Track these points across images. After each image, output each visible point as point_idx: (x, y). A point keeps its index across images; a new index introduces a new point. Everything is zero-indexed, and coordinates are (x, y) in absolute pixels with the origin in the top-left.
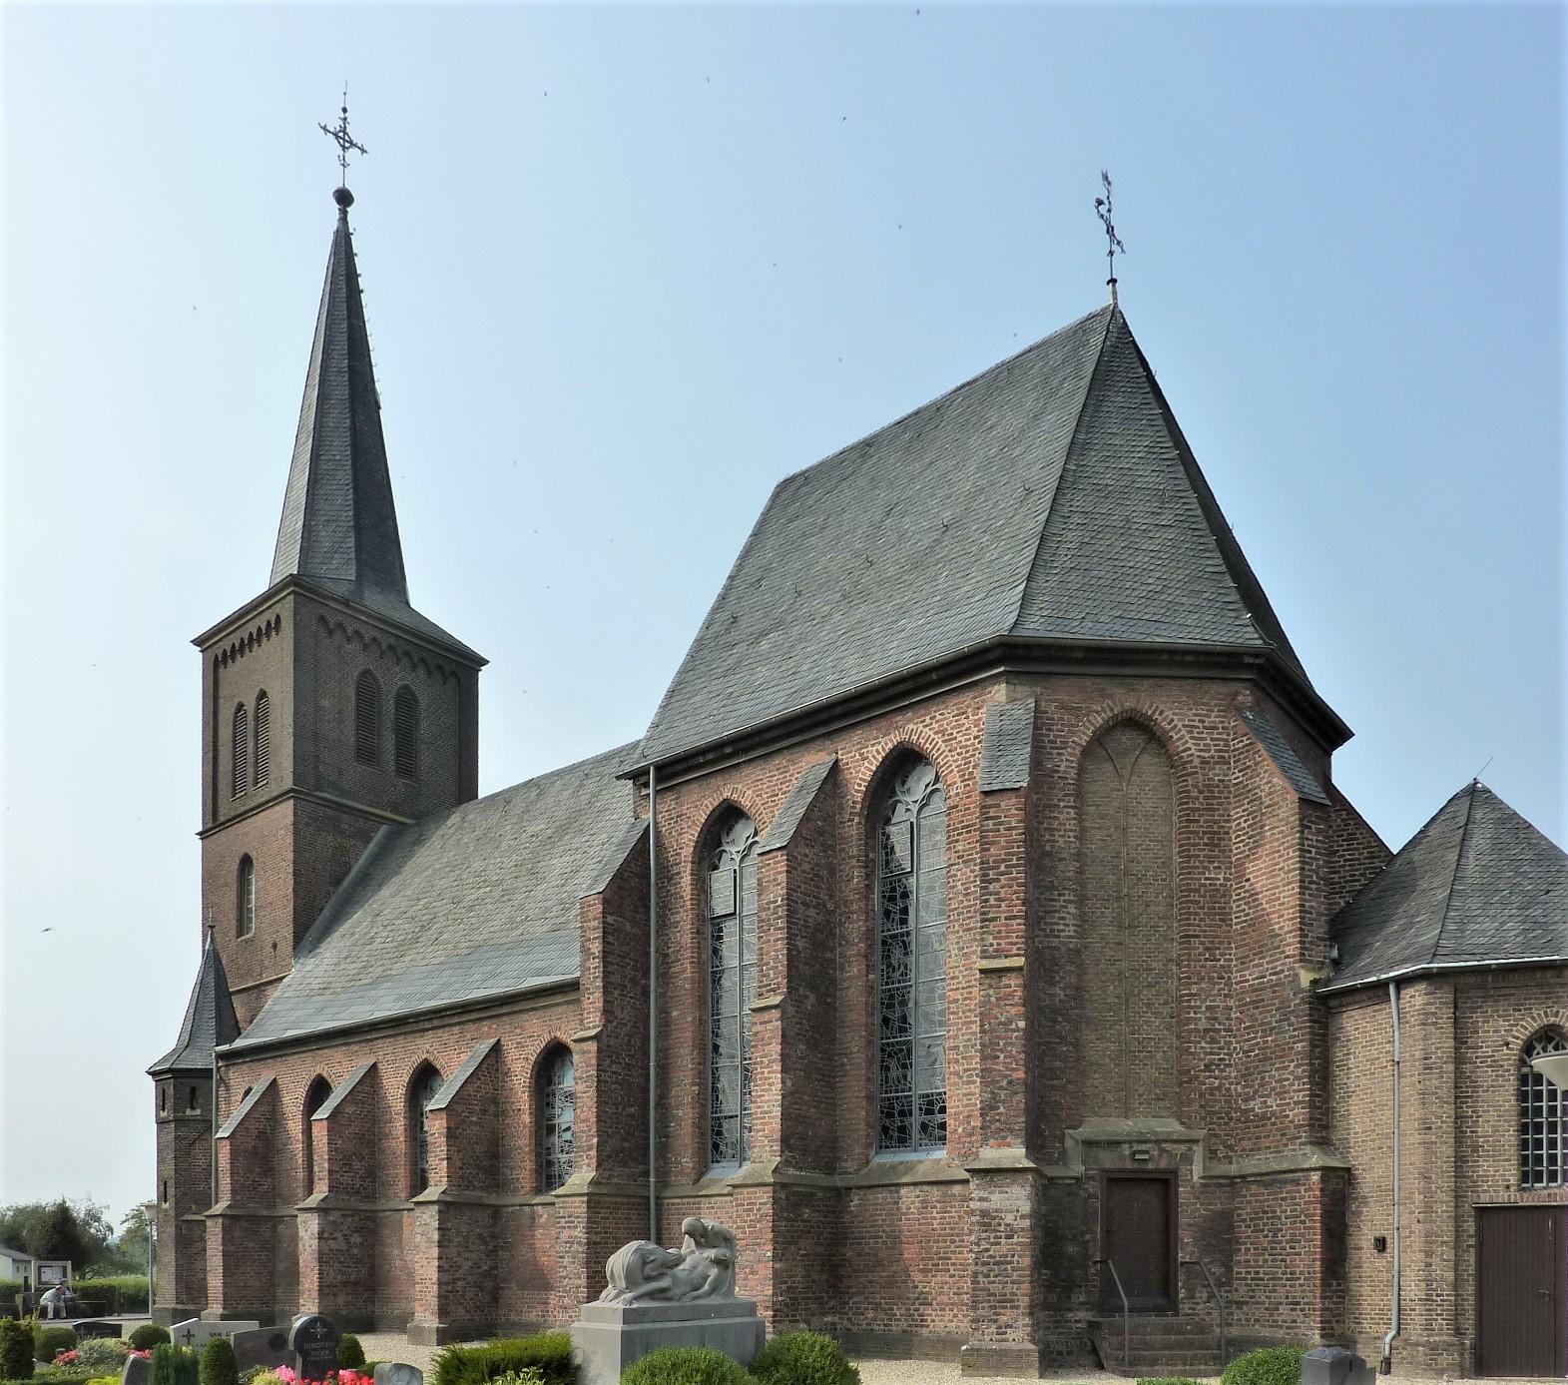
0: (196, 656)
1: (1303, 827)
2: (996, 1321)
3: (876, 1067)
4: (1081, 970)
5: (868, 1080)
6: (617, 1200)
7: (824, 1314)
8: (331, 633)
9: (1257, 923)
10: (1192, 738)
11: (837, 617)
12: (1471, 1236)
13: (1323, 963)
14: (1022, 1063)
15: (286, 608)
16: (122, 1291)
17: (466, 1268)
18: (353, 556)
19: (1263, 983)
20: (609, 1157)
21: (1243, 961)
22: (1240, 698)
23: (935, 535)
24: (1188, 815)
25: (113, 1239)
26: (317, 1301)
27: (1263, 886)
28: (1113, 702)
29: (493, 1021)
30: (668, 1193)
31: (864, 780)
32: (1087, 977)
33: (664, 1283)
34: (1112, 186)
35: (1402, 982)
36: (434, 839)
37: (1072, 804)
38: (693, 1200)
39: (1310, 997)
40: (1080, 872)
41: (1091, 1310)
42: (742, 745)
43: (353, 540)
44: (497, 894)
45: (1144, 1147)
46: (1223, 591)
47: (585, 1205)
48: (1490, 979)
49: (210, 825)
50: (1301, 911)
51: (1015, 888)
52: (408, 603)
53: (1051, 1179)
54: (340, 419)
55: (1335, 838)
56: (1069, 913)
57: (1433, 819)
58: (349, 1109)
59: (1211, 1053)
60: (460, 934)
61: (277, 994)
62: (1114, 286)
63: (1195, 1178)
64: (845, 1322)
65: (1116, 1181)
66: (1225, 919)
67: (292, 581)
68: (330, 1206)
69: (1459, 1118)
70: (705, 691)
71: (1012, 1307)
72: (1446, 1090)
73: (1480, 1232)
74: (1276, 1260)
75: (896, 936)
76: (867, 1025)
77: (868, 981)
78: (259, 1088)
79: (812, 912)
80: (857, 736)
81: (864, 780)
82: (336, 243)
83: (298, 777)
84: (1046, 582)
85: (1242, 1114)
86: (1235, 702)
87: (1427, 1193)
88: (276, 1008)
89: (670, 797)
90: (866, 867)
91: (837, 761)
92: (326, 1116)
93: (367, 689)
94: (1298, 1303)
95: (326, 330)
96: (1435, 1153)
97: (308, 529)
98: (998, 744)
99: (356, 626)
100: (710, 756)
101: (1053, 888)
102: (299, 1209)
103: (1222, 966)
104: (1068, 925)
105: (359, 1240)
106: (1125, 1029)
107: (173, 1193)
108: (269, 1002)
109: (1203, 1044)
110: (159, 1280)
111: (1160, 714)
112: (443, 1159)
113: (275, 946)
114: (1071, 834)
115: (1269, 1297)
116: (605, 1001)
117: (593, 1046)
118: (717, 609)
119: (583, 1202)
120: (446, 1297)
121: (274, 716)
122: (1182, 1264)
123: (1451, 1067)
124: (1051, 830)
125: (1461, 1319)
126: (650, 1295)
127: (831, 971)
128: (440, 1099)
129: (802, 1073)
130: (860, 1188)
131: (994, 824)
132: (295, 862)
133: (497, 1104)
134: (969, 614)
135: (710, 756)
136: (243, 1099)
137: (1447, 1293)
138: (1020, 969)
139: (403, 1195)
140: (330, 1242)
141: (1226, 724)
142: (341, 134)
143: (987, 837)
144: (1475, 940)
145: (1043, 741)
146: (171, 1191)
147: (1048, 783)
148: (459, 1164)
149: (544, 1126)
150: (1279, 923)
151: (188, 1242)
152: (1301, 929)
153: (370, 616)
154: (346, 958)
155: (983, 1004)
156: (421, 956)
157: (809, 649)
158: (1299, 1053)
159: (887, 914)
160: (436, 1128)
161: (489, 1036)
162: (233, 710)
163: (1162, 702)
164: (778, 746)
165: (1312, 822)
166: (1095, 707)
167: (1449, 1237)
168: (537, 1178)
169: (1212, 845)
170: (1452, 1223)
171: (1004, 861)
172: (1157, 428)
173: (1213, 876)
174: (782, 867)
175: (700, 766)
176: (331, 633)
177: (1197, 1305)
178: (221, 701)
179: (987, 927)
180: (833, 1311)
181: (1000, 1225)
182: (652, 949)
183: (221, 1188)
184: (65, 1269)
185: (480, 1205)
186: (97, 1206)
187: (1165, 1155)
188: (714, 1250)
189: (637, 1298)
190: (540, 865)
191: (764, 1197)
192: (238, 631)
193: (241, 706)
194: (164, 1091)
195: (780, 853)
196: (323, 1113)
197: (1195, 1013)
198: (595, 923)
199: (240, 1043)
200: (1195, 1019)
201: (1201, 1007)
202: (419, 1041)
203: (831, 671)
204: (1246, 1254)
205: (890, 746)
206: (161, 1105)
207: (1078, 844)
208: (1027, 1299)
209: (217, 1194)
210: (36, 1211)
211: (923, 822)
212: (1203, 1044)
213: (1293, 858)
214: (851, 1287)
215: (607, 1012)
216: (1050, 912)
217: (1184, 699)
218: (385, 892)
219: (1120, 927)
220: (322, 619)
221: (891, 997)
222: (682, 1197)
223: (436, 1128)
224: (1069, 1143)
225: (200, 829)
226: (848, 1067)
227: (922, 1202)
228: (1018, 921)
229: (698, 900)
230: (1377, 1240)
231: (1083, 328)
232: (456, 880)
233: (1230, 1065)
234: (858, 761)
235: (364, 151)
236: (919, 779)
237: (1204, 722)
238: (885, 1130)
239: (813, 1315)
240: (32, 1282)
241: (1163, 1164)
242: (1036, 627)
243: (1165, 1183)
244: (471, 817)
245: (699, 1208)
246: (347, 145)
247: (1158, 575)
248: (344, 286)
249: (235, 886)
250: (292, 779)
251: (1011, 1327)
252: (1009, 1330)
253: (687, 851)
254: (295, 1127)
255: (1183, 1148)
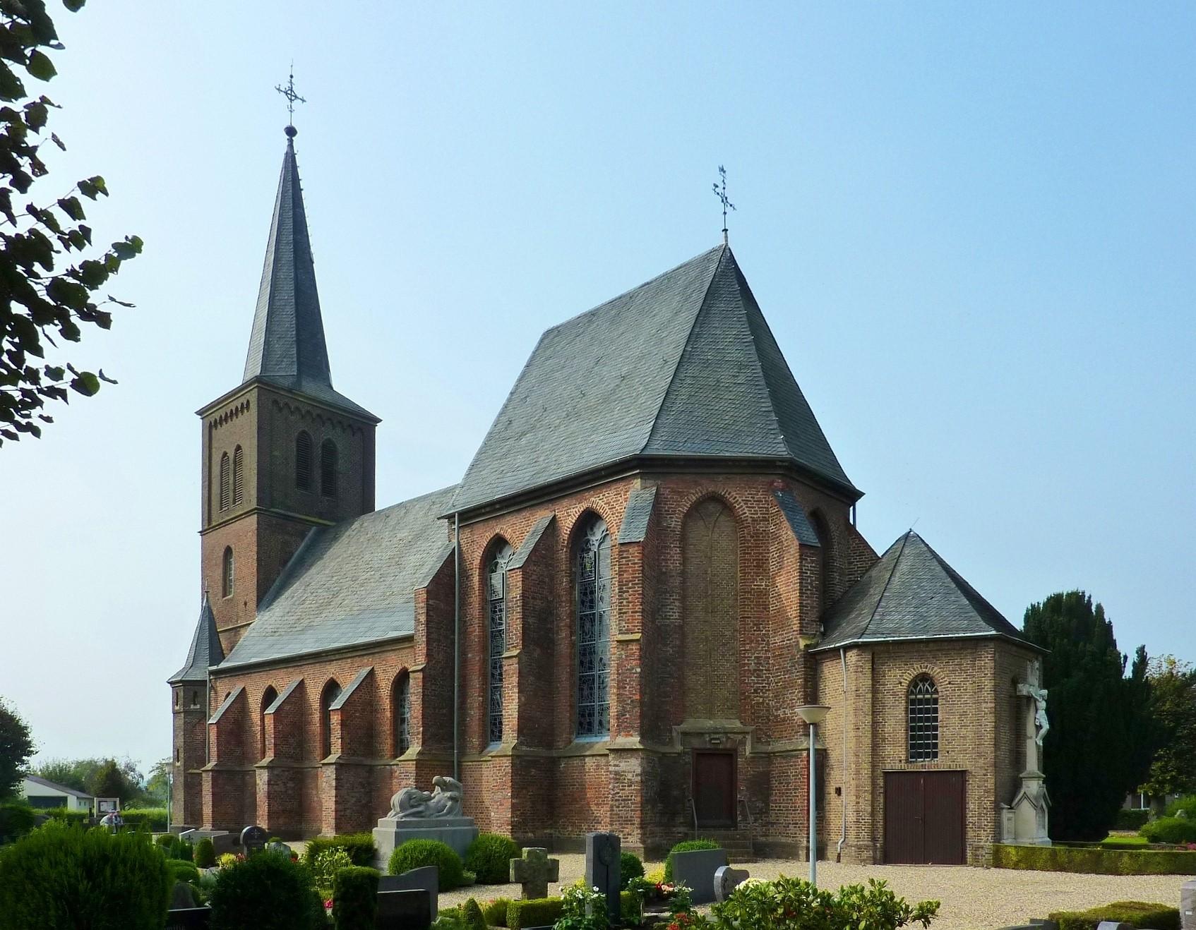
0: (198, 421)
1: (801, 559)
2: (622, 831)
3: (576, 689)
4: (683, 636)
5: (571, 696)
6: (435, 763)
7: (544, 828)
8: (280, 410)
9: (781, 612)
10: (747, 507)
11: (562, 428)
12: (881, 787)
13: (815, 634)
14: (638, 690)
15: (253, 397)
16: (150, 817)
17: (353, 802)
18: (295, 359)
19: (783, 645)
20: (429, 738)
21: (775, 631)
22: (775, 484)
23: (618, 382)
24: (745, 550)
25: (143, 784)
26: (267, 822)
27: (783, 591)
28: (702, 488)
29: (371, 656)
30: (466, 759)
31: (569, 528)
32: (688, 640)
33: (420, 809)
34: (726, 173)
35: (847, 648)
36: (344, 537)
37: (678, 545)
38: (478, 763)
39: (804, 654)
40: (684, 582)
41: (686, 826)
42: (505, 504)
43: (295, 349)
44: (377, 576)
45: (717, 736)
46: (768, 422)
47: (415, 766)
48: (891, 648)
49: (206, 527)
50: (800, 606)
51: (637, 596)
52: (332, 388)
53: (663, 754)
54: (288, 273)
55: (852, 555)
56: (676, 606)
57: (887, 551)
58: (287, 708)
59: (758, 683)
60: (354, 601)
61: (246, 634)
62: (726, 233)
63: (747, 754)
64: (557, 833)
65: (701, 755)
66: (766, 608)
67: (258, 379)
68: (274, 765)
69: (875, 724)
70: (490, 467)
71: (631, 824)
72: (867, 708)
73: (885, 782)
74: (787, 800)
75: (587, 615)
76: (570, 666)
77: (571, 640)
78: (235, 693)
79: (538, 602)
80: (565, 502)
81: (569, 528)
82: (286, 161)
83: (260, 500)
84: (667, 419)
85: (775, 718)
86: (773, 487)
87: (857, 763)
88: (246, 643)
89: (467, 531)
90: (570, 577)
91: (555, 516)
92: (273, 712)
93: (304, 442)
94: (797, 824)
95: (279, 216)
96: (861, 742)
97: (267, 342)
98: (634, 512)
99: (297, 404)
100: (488, 509)
101: (665, 593)
102: (257, 767)
103: (765, 634)
104: (675, 613)
105: (293, 785)
106: (709, 669)
107: (182, 756)
108: (241, 640)
109: (753, 678)
110: (173, 810)
111: (729, 494)
112: (338, 739)
113: (246, 604)
114: (678, 562)
115: (785, 820)
116: (428, 649)
117: (420, 675)
118: (502, 413)
119: (413, 764)
120: (339, 819)
121: (245, 462)
122: (740, 801)
123: (870, 695)
124: (666, 560)
125: (876, 832)
126: (413, 815)
127: (550, 635)
128: (336, 704)
129: (531, 693)
130: (566, 757)
131: (626, 561)
132: (258, 553)
133: (372, 706)
134: (626, 436)
135: (488, 509)
136: (225, 699)
137: (868, 818)
138: (637, 640)
139: (318, 758)
140: (275, 787)
141: (767, 499)
142: (289, 92)
143: (622, 568)
144: (887, 626)
145: (662, 511)
146: (182, 755)
147: (664, 534)
148: (348, 741)
149: (399, 718)
150: (790, 612)
151: (192, 787)
152: (800, 616)
153: (307, 398)
154: (288, 613)
155: (619, 659)
156: (331, 614)
157: (545, 447)
158: (799, 685)
159: (583, 602)
160: (335, 719)
161: (367, 666)
162: (221, 456)
163: (729, 488)
164: (525, 505)
165: (808, 556)
166: (692, 491)
167: (868, 788)
168: (394, 750)
169: (758, 566)
170: (870, 780)
171: (631, 581)
172: (743, 323)
173: (759, 583)
174: (520, 578)
175: (484, 514)
176: (280, 410)
177: (749, 826)
178: (214, 450)
179: (622, 617)
180: (551, 827)
181: (625, 779)
182: (456, 618)
183: (211, 753)
184: (115, 802)
185: (360, 765)
186: (133, 761)
187: (730, 740)
188: (450, 793)
189: (405, 816)
190: (403, 559)
191: (507, 763)
192: (224, 408)
193: (225, 454)
194: (177, 693)
195: (518, 570)
196: (271, 710)
197: (748, 660)
198: (422, 605)
199: (223, 665)
200: (748, 664)
201: (751, 657)
202: (328, 667)
203: (554, 463)
204: (775, 796)
205: (582, 509)
206: (176, 702)
207: (682, 568)
208: (639, 820)
209: (209, 757)
210: (92, 765)
211: (601, 552)
212: (753, 678)
213: (796, 576)
214: (560, 813)
215: (429, 655)
216: (664, 606)
217: (743, 485)
218: (313, 570)
219: (707, 612)
220: (275, 402)
221: (585, 650)
222: (472, 762)
223: (335, 719)
224: (674, 734)
225: (201, 530)
226: (560, 689)
227: (596, 766)
228: (638, 614)
229: (483, 590)
230: (836, 789)
231: (706, 258)
232: (354, 566)
233: (769, 690)
234: (565, 516)
235: (303, 101)
236: (599, 528)
237: (754, 498)
238: (581, 724)
239: (537, 828)
240: (95, 811)
241: (728, 746)
242: (658, 449)
243: (729, 756)
244: (365, 524)
245: (481, 768)
246: (293, 98)
247: (732, 414)
248: (291, 188)
249: (222, 566)
250: (256, 502)
251: (631, 835)
252: (629, 837)
253: (477, 562)
254: (256, 716)
255: (740, 737)
